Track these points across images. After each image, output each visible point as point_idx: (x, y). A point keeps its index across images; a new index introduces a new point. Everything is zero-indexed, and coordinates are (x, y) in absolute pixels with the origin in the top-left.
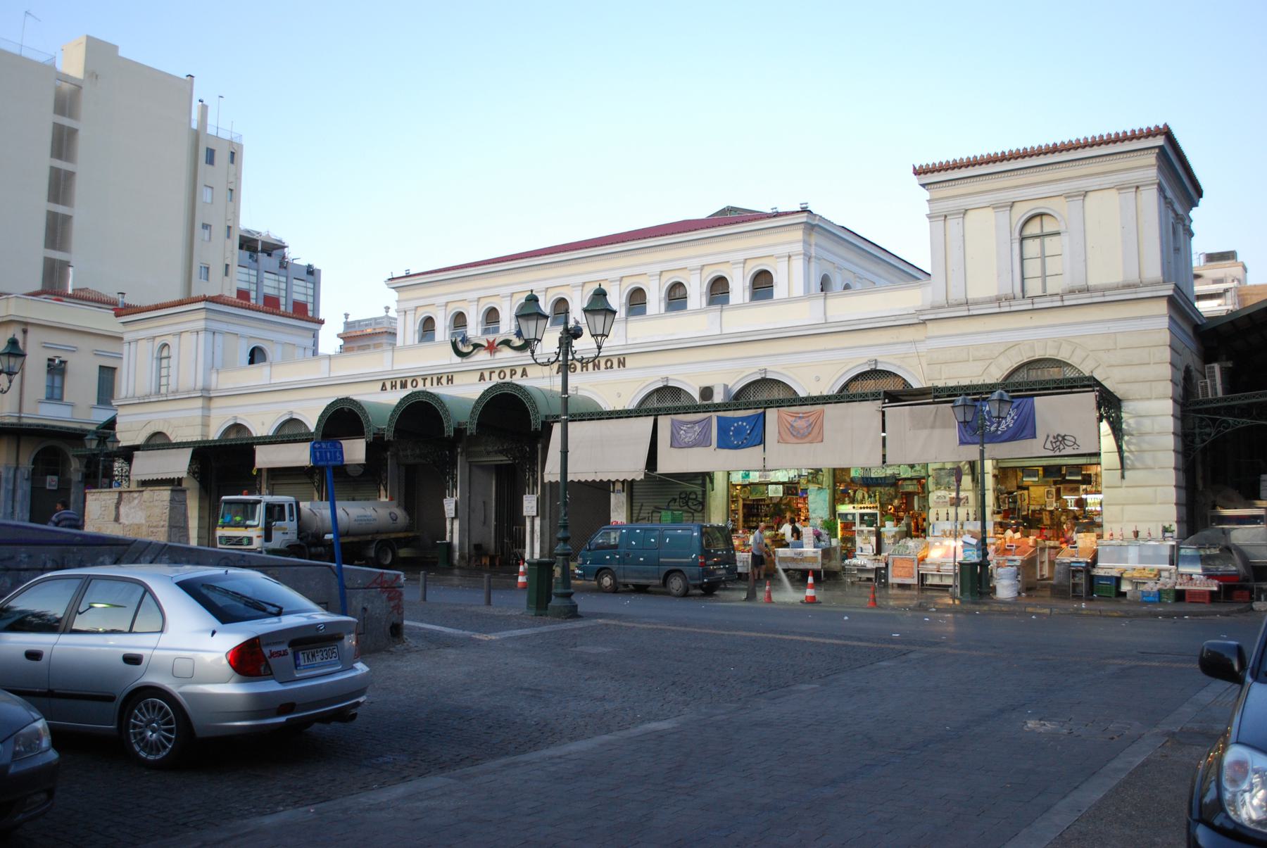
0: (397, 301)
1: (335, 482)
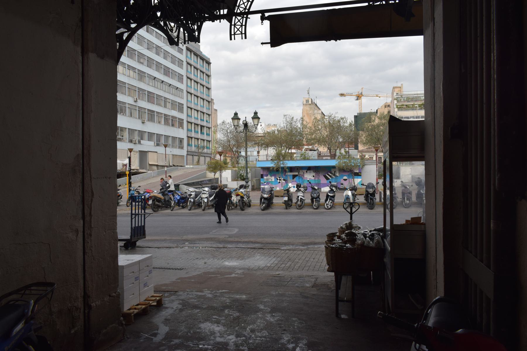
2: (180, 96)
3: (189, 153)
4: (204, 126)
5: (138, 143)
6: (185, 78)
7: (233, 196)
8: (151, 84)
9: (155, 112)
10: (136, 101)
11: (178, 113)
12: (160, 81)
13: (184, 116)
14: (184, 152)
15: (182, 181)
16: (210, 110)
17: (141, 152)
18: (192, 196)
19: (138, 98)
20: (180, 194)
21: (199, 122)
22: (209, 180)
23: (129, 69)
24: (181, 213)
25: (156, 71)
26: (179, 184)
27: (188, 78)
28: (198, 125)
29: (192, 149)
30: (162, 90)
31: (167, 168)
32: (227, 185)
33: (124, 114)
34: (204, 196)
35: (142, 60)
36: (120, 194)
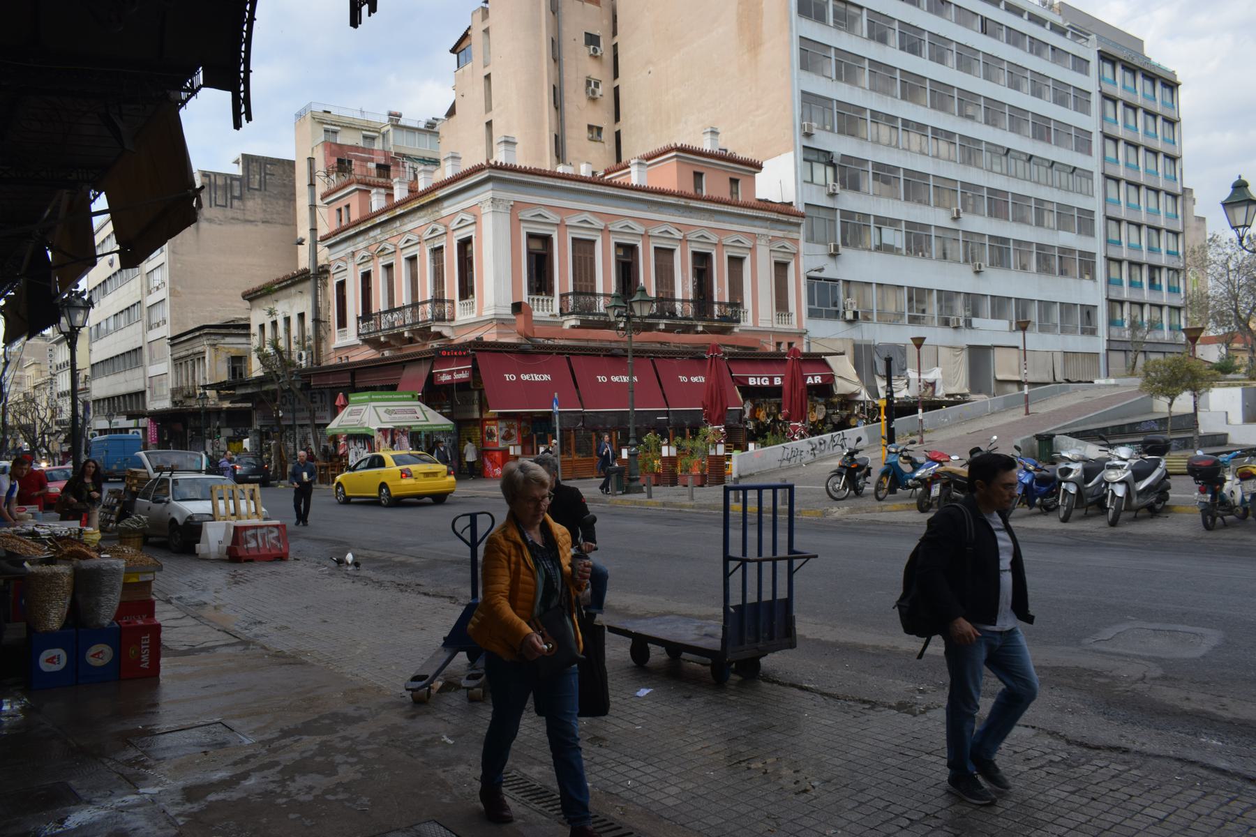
0: (1225, 204)
1: (137, 363)
2: (1084, 189)
3: (1115, 346)
4: (1160, 268)
5: (966, 326)
6: (1096, 140)
7: (1229, 477)
8: (997, 168)
9: (1011, 241)
10: (956, 219)
11: (1079, 237)
12: (1024, 158)
13: (1096, 245)
14: (1099, 344)
15: (1066, 423)
16: (1180, 218)
17: (972, 348)
18: (1071, 476)
19: (961, 211)
20: (1031, 468)
21: (1144, 257)
22: (1160, 419)
23: (937, 139)
24: (1033, 530)
25: (1010, 131)
26: (1052, 433)
27: (1106, 136)
28: (1140, 265)
29: (1123, 335)
30: (1030, 181)
31: (1029, 388)
32: (1226, 435)
33: (927, 255)
34: (1113, 475)
35: (970, 111)
36: (861, 463)
